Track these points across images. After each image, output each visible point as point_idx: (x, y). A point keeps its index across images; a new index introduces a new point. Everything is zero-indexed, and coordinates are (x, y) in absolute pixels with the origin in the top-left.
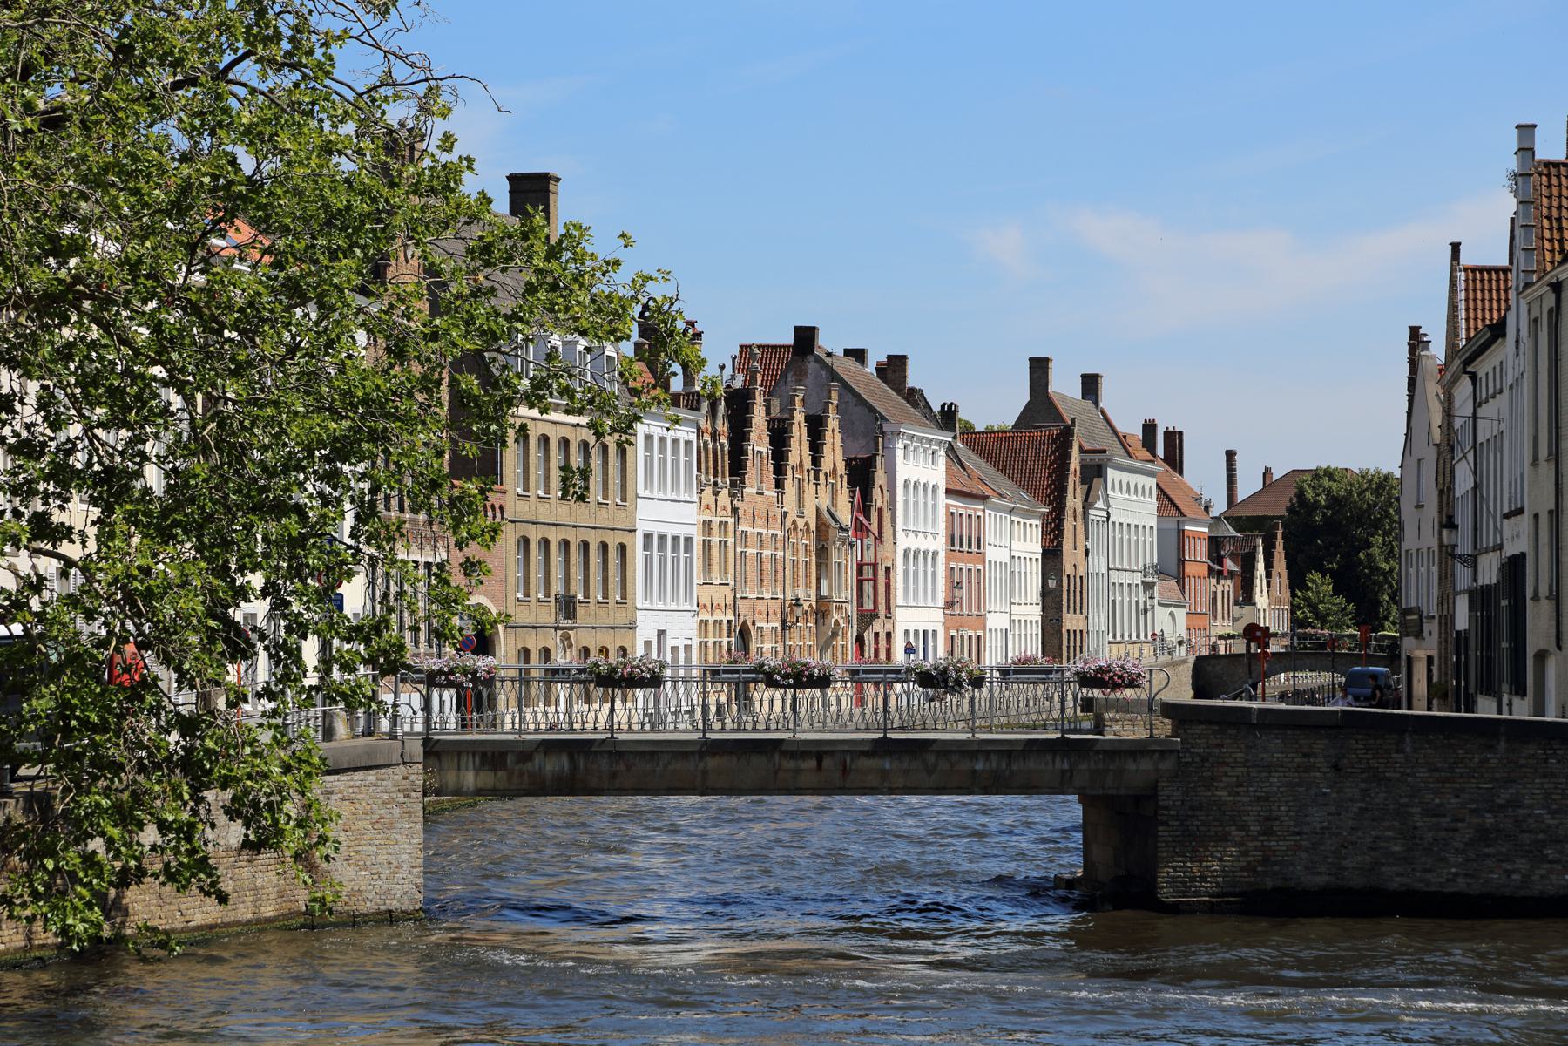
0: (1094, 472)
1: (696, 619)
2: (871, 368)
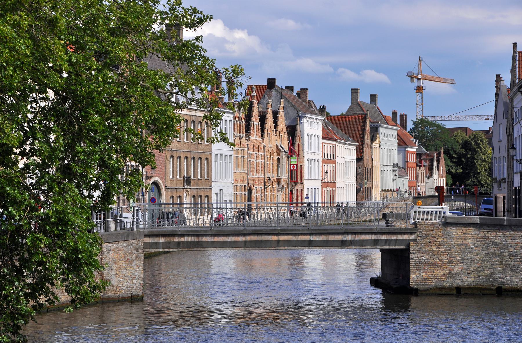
0: (374, 131)
1: (233, 185)
2: (295, 93)
